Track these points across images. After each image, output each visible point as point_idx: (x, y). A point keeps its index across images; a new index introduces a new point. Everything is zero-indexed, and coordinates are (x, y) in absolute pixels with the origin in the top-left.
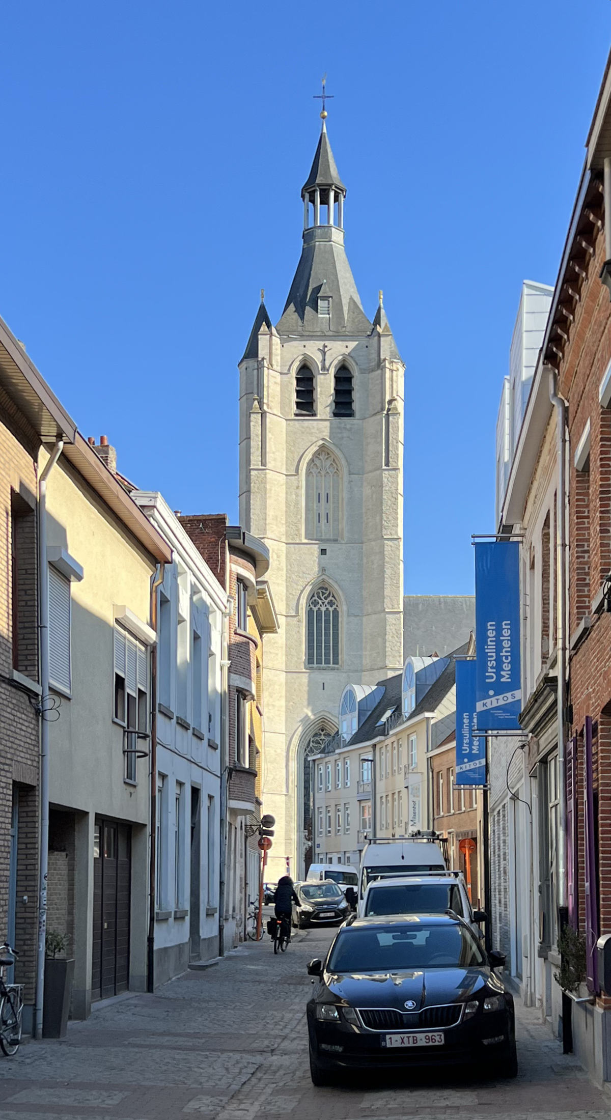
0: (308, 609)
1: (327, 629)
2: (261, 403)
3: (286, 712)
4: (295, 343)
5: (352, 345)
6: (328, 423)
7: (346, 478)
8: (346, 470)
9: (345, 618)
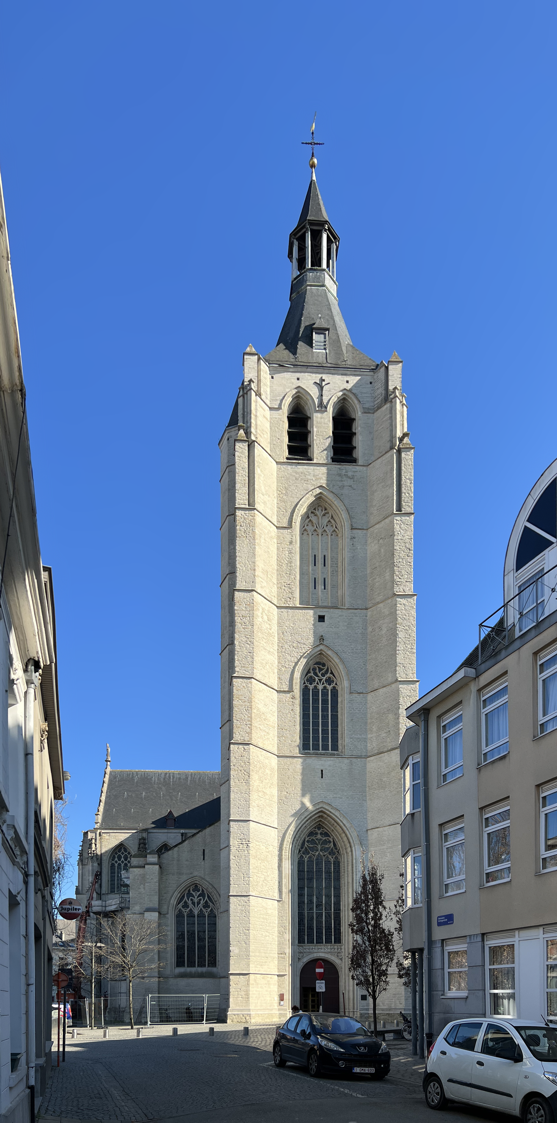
0: (303, 686)
1: (325, 709)
2: (248, 433)
3: (279, 803)
4: (287, 375)
5: (354, 380)
6: (324, 469)
7: (347, 532)
8: (347, 525)
9: (346, 696)
